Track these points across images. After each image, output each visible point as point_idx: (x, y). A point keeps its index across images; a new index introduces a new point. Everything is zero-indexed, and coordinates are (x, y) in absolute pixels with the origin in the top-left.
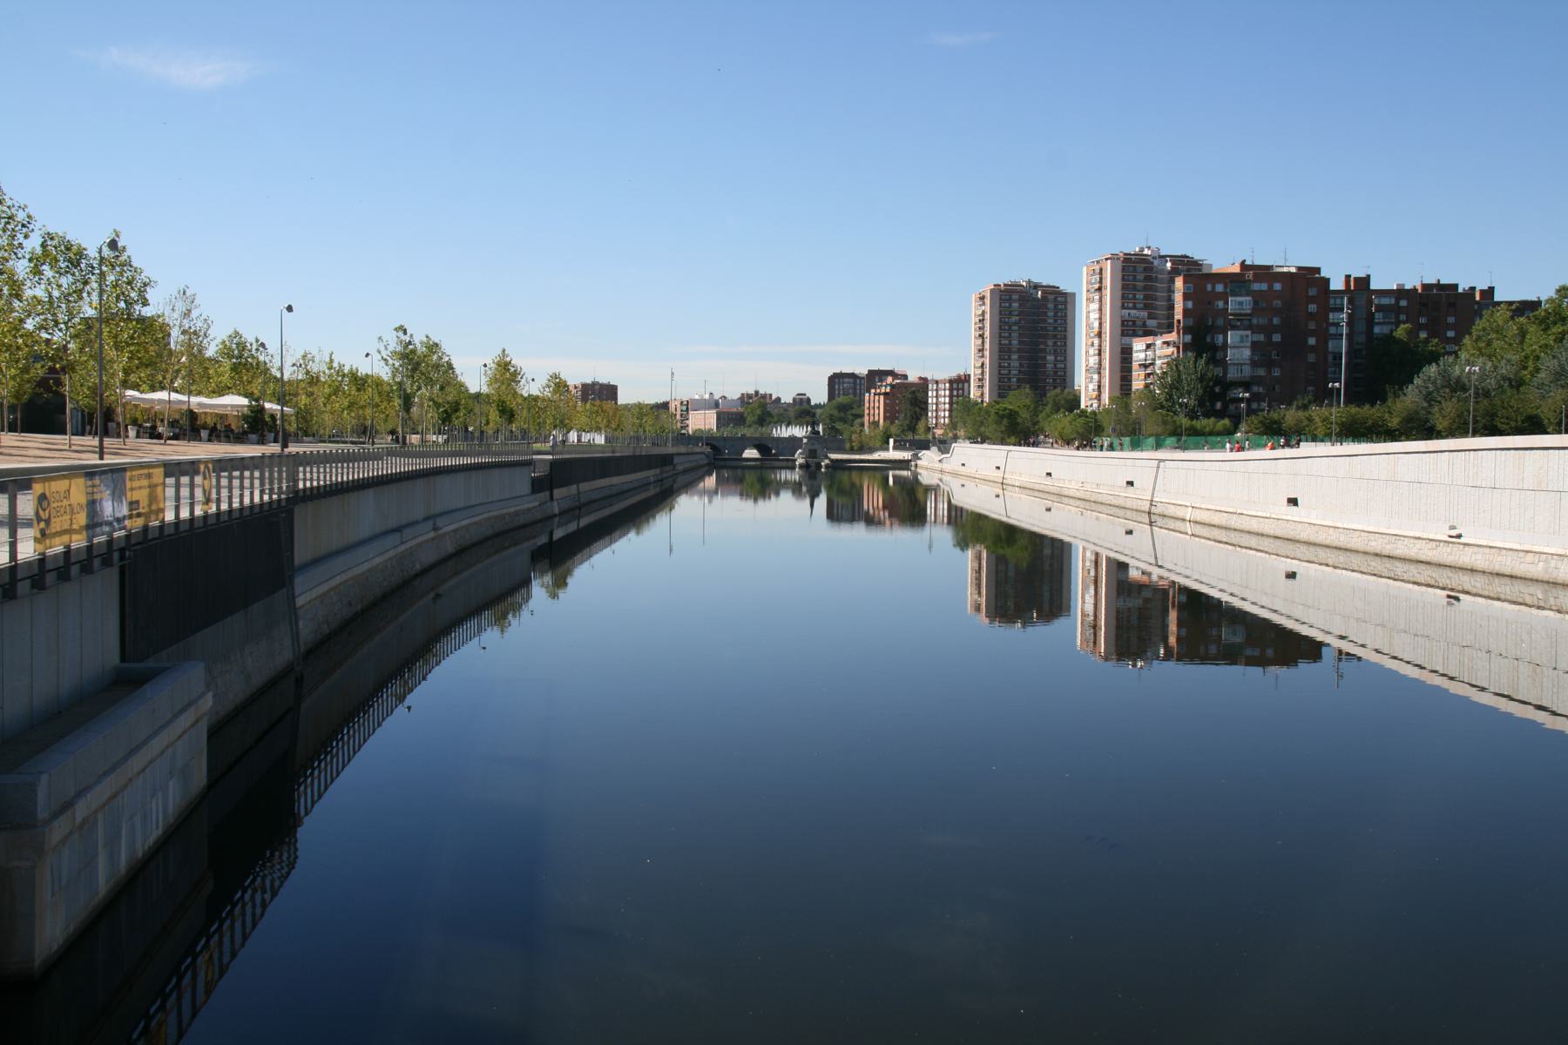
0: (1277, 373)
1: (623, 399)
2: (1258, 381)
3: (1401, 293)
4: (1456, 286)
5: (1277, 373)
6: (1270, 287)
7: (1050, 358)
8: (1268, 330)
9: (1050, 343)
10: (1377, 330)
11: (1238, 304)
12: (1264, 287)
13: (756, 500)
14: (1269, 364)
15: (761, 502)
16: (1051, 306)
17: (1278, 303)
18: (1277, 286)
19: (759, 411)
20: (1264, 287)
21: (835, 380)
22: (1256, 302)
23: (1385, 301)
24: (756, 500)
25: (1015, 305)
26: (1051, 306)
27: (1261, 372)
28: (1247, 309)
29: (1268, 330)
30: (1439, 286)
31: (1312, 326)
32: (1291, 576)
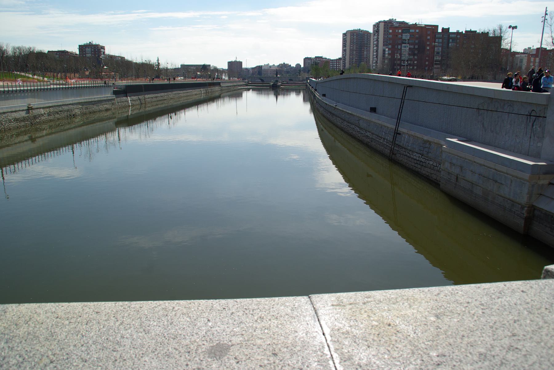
0: (416, 57)
1: (244, 66)
2: (410, 60)
3: (458, 33)
4: (437, 27)
5: (416, 57)
6: (415, 31)
7: (365, 53)
8: (414, 44)
9: (365, 48)
10: (450, 45)
11: (406, 36)
12: (413, 31)
13: (277, 96)
14: (414, 55)
15: (285, 96)
16: (366, 37)
17: (417, 36)
18: (417, 31)
19: (284, 69)
20: (413, 31)
21: (306, 60)
22: (411, 36)
23: (453, 36)
24: (277, 96)
25: (355, 37)
26: (366, 37)
27: (412, 57)
28: (408, 37)
29: (414, 44)
30: (471, 31)
31: (428, 43)
32: (373, 110)
